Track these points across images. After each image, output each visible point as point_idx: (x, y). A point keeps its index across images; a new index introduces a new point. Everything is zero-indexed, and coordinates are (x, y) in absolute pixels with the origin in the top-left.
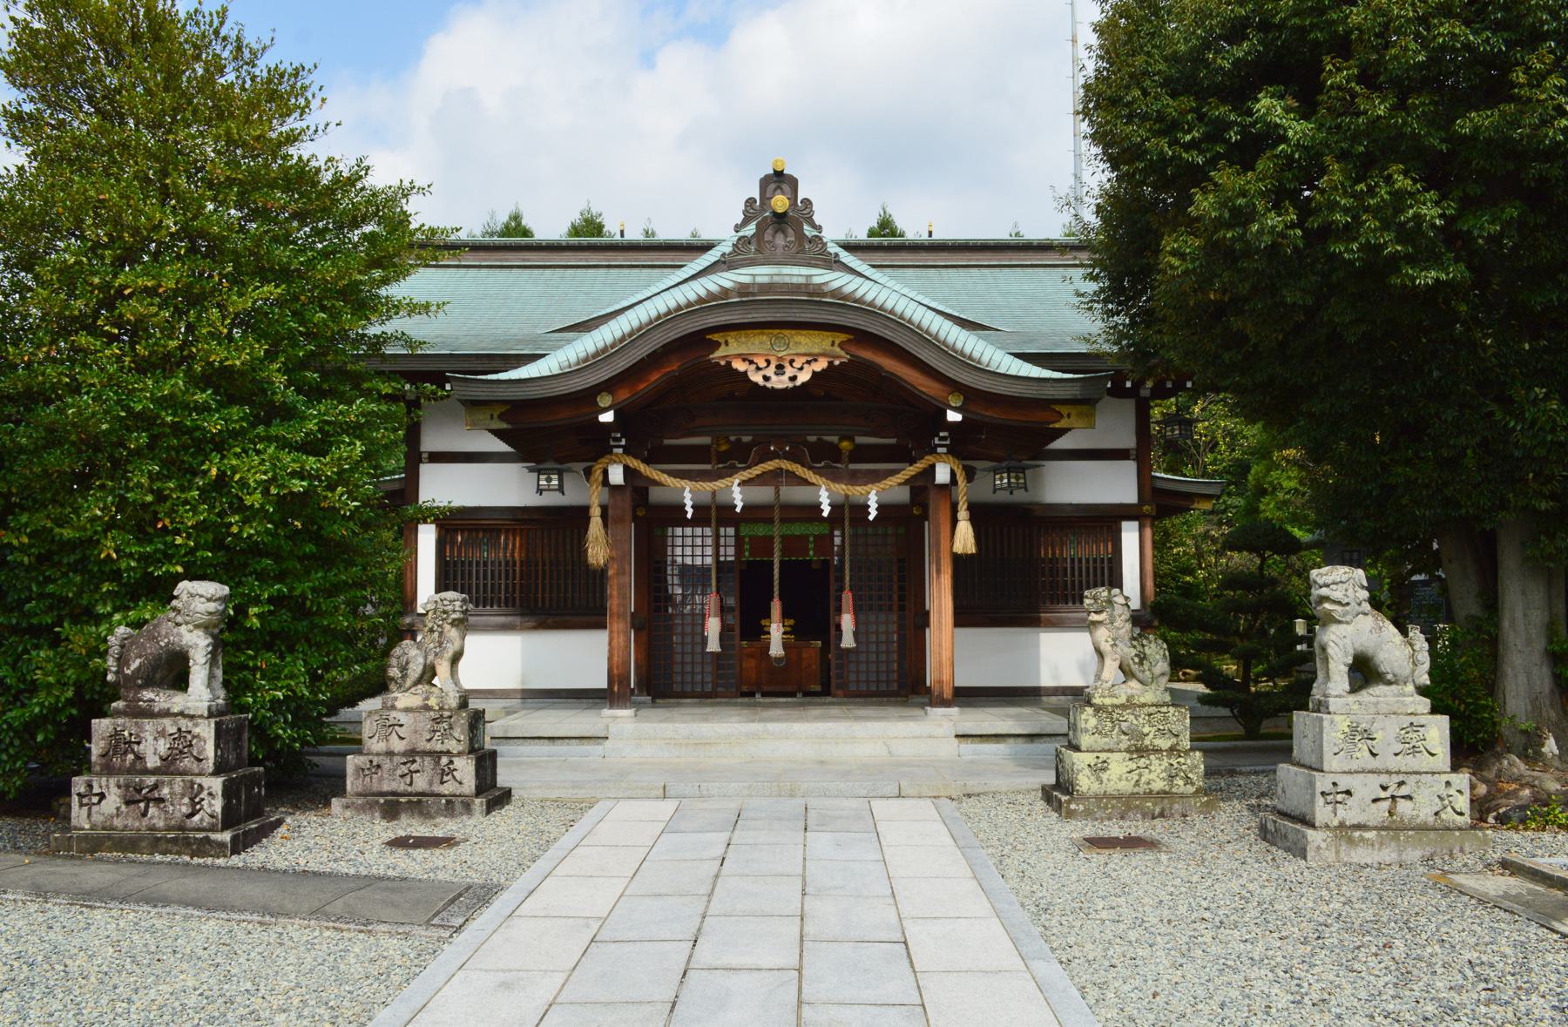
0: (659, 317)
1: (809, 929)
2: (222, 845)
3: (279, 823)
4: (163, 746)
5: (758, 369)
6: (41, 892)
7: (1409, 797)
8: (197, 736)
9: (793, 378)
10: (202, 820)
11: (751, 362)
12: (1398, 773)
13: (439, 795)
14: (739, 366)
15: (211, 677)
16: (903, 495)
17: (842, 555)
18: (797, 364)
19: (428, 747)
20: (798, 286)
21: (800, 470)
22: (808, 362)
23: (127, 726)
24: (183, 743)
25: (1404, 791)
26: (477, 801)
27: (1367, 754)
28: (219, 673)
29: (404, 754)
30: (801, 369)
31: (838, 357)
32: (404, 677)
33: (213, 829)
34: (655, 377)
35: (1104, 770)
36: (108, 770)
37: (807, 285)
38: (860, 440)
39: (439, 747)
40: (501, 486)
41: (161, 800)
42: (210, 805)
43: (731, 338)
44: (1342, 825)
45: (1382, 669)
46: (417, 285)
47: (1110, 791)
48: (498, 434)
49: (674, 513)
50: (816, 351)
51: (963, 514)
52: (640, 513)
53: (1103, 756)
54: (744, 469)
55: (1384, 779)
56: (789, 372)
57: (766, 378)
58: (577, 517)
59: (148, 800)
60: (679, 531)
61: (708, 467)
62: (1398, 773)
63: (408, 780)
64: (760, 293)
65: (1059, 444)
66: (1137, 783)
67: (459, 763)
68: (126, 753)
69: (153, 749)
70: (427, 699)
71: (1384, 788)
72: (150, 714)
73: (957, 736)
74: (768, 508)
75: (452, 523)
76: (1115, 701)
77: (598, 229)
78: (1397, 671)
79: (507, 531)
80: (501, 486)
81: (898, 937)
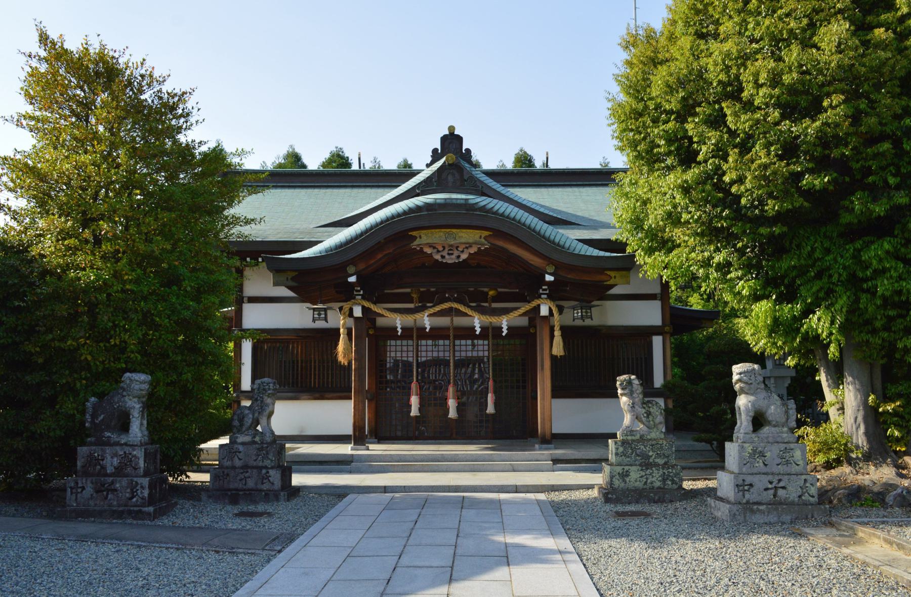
1: (459, 551)
2: (149, 514)
3: (176, 504)
4: (116, 461)
5: (438, 251)
6: (61, 538)
7: (783, 488)
8: (135, 456)
9: (459, 257)
10: (137, 501)
11: (434, 248)
12: (778, 474)
13: (261, 490)
14: (428, 250)
15: (142, 424)
16: (524, 322)
18: (460, 249)
19: (255, 464)
21: (462, 308)
22: (467, 248)
23: (97, 452)
24: (127, 462)
25: (781, 484)
26: (282, 494)
27: (762, 464)
28: (145, 422)
29: (242, 468)
30: (463, 252)
31: (483, 245)
32: (242, 425)
33: (143, 505)
34: (380, 256)
35: (628, 476)
36: (86, 474)
38: (500, 290)
39: (261, 464)
40: (295, 316)
41: (116, 490)
42: (142, 493)
44: (748, 502)
45: (770, 418)
46: (247, 206)
48: (290, 288)
49: (390, 332)
50: (471, 241)
51: (557, 333)
52: (371, 332)
53: (626, 468)
54: (431, 307)
55: (770, 477)
56: (456, 253)
57: (443, 257)
58: (334, 334)
59: (108, 490)
60: (393, 343)
61: (411, 306)
62: (778, 474)
63: (244, 482)
65: (613, 291)
66: (646, 483)
67: (272, 472)
68: (96, 465)
69: (111, 463)
71: (771, 483)
72: (108, 443)
74: (447, 329)
76: (633, 438)
77: (346, 163)
78: (778, 420)
79: (293, 343)
80: (295, 316)
81: (504, 554)
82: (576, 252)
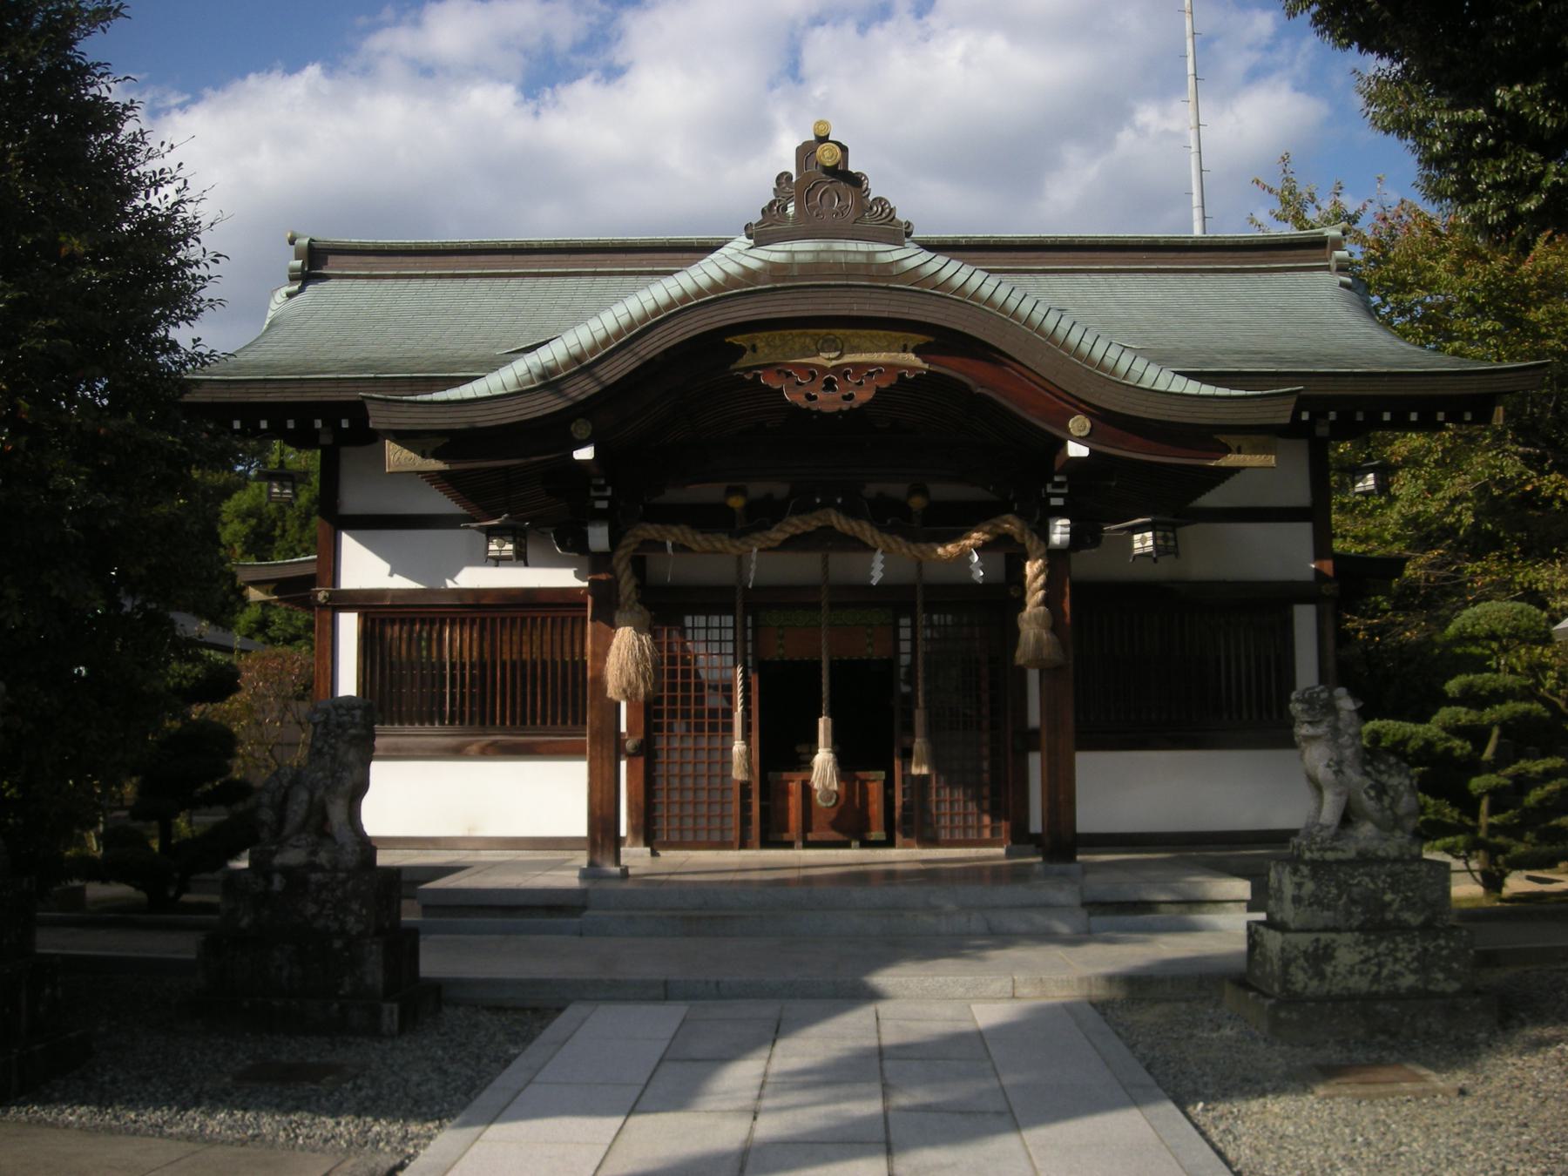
0: (657, 311)
17: (911, 678)
20: (857, 265)
26: (386, 1007)
32: (281, 820)
37: (868, 265)
43: (761, 339)
47: (1336, 990)
53: (1325, 937)
57: (810, 398)
64: (802, 277)
65: (1208, 500)
66: (1376, 978)
70: (314, 853)
73: (1084, 905)
75: (369, 604)
76: (1340, 855)
82: (1146, 385)
